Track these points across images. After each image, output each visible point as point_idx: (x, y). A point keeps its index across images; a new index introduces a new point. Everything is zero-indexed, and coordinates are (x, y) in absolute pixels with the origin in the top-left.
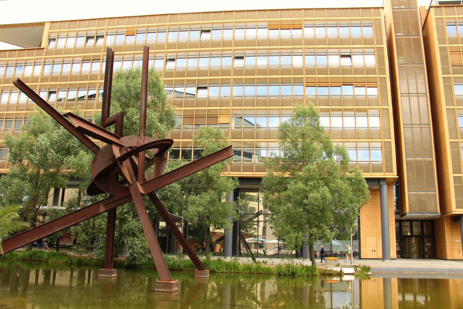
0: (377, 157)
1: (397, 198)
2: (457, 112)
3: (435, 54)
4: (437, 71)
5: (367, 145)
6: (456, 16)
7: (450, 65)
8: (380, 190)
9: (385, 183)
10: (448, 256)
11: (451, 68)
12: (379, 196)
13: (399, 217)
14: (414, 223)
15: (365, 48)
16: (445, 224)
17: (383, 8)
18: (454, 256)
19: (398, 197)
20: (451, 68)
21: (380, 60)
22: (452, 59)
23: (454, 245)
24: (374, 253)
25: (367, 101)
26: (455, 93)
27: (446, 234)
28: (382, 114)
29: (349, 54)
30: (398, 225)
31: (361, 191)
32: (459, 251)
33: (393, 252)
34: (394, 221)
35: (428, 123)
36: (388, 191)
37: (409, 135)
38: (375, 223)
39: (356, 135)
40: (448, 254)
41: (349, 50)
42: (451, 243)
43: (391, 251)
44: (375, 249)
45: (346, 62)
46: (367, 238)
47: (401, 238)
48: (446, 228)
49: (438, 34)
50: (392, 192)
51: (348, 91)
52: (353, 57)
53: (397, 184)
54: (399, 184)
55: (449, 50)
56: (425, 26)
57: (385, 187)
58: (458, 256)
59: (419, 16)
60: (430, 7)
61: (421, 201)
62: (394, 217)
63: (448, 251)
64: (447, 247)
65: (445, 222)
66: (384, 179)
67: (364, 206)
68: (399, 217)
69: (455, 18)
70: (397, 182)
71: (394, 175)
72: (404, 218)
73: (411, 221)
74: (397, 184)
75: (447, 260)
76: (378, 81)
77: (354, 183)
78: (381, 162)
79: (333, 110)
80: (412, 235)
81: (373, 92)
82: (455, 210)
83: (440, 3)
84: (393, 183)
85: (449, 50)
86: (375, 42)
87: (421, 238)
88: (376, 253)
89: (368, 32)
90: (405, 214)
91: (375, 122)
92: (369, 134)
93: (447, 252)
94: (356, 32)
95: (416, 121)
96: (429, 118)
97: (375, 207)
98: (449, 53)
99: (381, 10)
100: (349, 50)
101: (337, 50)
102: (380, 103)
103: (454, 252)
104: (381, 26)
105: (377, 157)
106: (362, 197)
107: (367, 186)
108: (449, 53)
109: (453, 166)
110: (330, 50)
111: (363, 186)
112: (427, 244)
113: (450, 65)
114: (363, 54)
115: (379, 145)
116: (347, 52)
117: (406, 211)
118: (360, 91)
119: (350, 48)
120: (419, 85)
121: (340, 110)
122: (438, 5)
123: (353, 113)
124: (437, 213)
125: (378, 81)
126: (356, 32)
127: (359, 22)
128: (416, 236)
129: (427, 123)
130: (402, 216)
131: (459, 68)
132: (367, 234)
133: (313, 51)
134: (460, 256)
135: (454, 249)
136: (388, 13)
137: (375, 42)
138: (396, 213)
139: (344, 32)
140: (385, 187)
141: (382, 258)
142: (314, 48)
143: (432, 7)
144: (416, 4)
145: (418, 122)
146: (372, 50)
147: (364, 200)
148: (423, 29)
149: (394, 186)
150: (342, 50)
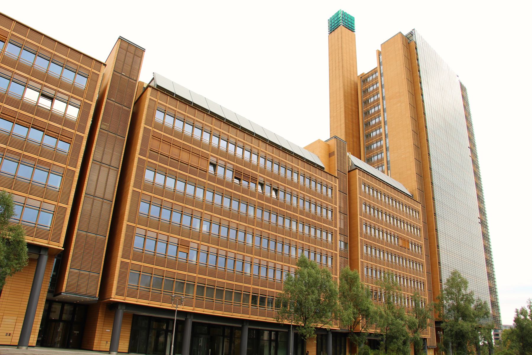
0: (46, 220)
1: (55, 273)
2: (142, 197)
3: (139, 133)
4: (136, 149)
5: (38, 204)
6: (167, 105)
7: (149, 149)
8: (38, 261)
9: (47, 253)
10: (94, 346)
11: (148, 151)
12: (35, 268)
13: (51, 297)
14: (66, 307)
15: (72, 97)
16: (100, 310)
17: (105, 65)
18: (101, 347)
19: (56, 274)
20: (148, 151)
21: (83, 115)
22: (154, 144)
23: (103, 335)
24: (8, 337)
25: (55, 155)
26: (145, 177)
27: (98, 322)
28: (66, 175)
29: (52, 96)
30: (48, 305)
31: (18, 256)
32: (107, 342)
33: (33, 338)
34: (45, 300)
35: (111, 199)
36: (47, 264)
37: (88, 207)
38: (20, 300)
39: (30, 188)
40: (95, 344)
41: (53, 92)
42: (101, 332)
43: (31, 336)
44: (11, 332)
45: (45, 103)
46: (4, 317)
47: (47, 323)
48: (99, 315)
49: (147, 115)
50: (51, 266)
51: (36, 135)
52: (56, 102)
53: (59, 258)
54: (61, 258)
55: (151, 134)
56: (138, 102)
57: (45, 258)
58: (104, 347)
59: (136, 90)
60: (149, 86)
61: (80, 282)
62: (46, 295)
63: (96, 341)
64: (96, 336)
65: (100, 308)
66: (46, 248)
67: (15, 275)
68: (51, 297)
69: (166, 106)
70: (59, 255)
71: (60, 246)
72: (57, 298)
73: (63, 303)
74: (59, 258)
75: (93, 350)
76: (74, 138)
77: (13, 245)
78: (49, 228)
79: (9, 151)
80: (60, 320)
81: (64, 147)
82: (115, 297)
83: (158, 86)
84: (55, 255)
85: (151, 134)
86: (85, 96)
87: (69, 325)
88: (10, 337)
89: (82, 82)
90: (60, 294)
91: (56, 182)
92: (45, 192)
93: (95, 341)
94: (68, 76)
95: (99, 193)
96: (113, 194)
97: (26, 279)
98: (151, 137)
99: (103, 66)
100: (53, 92)
101: (39, 86)
102: (68, 162)
103: (102, 342)
104: (97, 82)
105: (46, 220)
106: (17, 262)
107: (26, 249)
108: (151, 137)
109: (124, 250)
110: (31, 83)
111: (22, 249)
112: (75, 332)
113: (149, 149)
114: (68, 103)
115: (52, 208)
116: (51, 93)
117: (62, 289)
118: (50, 141)
119: (55, 90)
120: (114, 157)
121: (19, 154)
122: (155, 87)
123: (33, 163)
124: (95, 297)
125: (74, 138)
126: (68, 76)
127: (75, 67)
128: (64, 321)
129: (110, 199)
130: (55, 296)
131: (155, 154)
132: (5, 312)
133: (10, 74)
134: (107, 347)
135: (102, 339)
136: (108, 72)
137: (85, 96)
138: (49, 292)
139: (55, 70)
140: (45, 258)
141: (17, 344)
142: (12, 72)
143: (150, 87)
144: (137, 77)
145: (102, 196)
146: (79, 103)
147: (18, 266)
148: (135, 104)
149: (55, 259)
150: (45, 89)
